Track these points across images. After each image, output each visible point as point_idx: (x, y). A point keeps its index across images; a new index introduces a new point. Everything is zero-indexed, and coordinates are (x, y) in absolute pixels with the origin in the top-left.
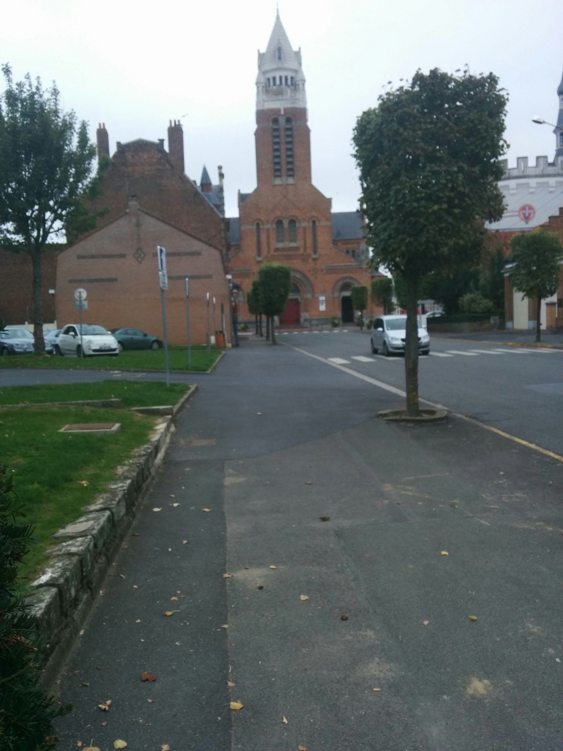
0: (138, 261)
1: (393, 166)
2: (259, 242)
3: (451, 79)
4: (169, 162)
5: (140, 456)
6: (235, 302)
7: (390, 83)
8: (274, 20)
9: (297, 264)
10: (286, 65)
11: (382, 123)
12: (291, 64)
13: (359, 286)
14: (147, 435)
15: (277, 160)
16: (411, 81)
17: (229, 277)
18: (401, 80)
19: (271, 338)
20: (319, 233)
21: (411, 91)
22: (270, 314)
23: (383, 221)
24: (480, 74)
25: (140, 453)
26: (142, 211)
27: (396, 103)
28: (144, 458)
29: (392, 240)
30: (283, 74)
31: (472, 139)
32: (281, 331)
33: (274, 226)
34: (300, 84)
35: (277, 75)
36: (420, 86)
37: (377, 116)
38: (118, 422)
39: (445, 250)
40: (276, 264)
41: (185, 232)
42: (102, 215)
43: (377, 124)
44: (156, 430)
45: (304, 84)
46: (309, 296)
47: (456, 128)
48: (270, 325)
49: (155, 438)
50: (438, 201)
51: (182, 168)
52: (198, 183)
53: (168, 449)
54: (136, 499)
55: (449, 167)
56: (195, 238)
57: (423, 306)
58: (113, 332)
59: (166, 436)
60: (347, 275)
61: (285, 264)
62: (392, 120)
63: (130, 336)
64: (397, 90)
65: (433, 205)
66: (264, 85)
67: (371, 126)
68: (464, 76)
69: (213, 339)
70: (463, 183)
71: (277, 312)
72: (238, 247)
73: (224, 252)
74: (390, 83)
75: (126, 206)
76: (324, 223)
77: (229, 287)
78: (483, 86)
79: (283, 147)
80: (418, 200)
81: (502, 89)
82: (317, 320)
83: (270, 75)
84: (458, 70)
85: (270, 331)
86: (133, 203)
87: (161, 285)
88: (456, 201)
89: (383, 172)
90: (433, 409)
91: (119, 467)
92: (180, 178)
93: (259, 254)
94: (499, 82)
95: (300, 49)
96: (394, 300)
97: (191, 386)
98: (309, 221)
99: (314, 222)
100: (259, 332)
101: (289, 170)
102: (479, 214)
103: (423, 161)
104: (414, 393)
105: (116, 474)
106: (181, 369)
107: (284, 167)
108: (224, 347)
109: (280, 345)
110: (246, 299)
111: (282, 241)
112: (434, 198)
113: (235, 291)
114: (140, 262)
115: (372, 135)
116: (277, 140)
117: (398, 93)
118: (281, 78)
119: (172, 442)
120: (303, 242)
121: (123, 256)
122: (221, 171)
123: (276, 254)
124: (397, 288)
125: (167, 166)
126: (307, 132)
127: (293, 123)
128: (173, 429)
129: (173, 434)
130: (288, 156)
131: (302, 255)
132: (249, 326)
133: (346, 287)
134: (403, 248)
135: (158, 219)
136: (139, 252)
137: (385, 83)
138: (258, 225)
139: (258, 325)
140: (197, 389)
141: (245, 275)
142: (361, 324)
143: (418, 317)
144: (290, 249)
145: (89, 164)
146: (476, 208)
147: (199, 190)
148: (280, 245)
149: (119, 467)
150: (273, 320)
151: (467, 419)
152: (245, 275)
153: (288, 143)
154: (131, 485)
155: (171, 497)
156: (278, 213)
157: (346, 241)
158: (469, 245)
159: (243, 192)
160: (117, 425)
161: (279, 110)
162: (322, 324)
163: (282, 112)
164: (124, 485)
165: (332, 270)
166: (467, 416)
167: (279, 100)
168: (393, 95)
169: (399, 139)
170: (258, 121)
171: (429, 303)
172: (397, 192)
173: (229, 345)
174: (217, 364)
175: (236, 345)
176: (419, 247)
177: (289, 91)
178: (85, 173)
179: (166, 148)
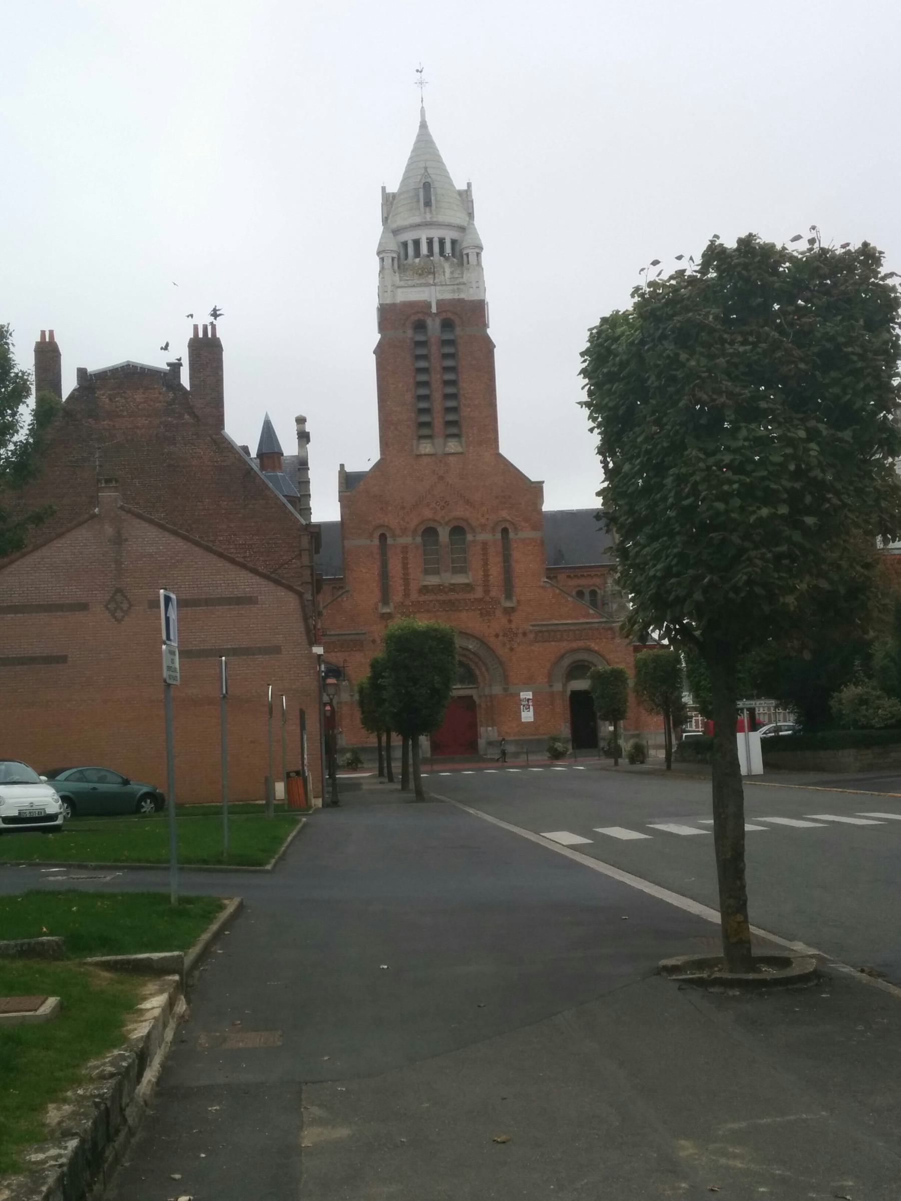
0: (115, 617)
1: (668, 427)
2: (384, 575)
3: (783, 256)
4: (191, 410)
5: (103, 1077)
6: (331, 704)
7: (655, 263)
8: (416, 130)
9: (470, 621)
10: (441, 218)
11: (642, 342)
12: (453, 215)
13: (608, 668)
14: (123, 1024)
15: (423, 391)
16: (698, 260)
17: (318, 650)
18: (679, 258)
19: (412, 785)
20: (516, 555)
21: (701, 280)
22: (410, 732)
23: (653, 538)
24: (843, 247)
25: (104, 1070)
26: (129, 511)
27: (669, 303)
28: (112, 1082)
29: (673, 580)
30: (436, 234)
31: (833, 374)
32: (436, 767)
33: (419, 539)
34: (472, 253)
35: (423, 235)
36: (718, 269)
37: (631, 326)
38: (53, 994)
39: (790, 600)
40: (422, 623)
41: (221, 555)
42: (38, 519)
43: (632, 343)
44: (142, 1012)
45: (478, 254)
46: (497, 690)
47: (797, 353)
48: (410, 754)
49: (140, 1030)
50: (769, 498)
51: (219, 421)
52: (254, 453)
53: (168, 1057)
54: (90, 1186)
55: (789, 430)
56: (244, 566)
57: (752, 711)
58: (52, 775)
59: (165, 1026)
60: (581, 644)
61: (442, 623)
62: (663, 337)
63: (91, 785)
64: (671, 278)
65: (759, 508)
66: (395, 255)
67: (621, 347)
68: (810, 250)
69: (280, 789)
70: (820, 463)
71: (426, 726)
72: (339, 585)
73: (308, 596)
74: (655, 263)
75: (94, 500)
76: (527, 533)
77: (320, 672)
78: (851, 269)
79: (436, 379)
80: (724, 497)
81: (892, 275)
82: (516, 742)
83: (409, 237)
84: (797, 238)
85: (411, 770)
86: (108, 495)
87: (165, 674)
88: (808, 499)
89: (649, 438)
90: (785, 954)
91: (51, 1106)
92: (214, 442)
93: (385, 601)
94: (883, 261)
95: (469, 185)
96: (687, 698)
97: (226, 902)
98: (493, 530)
99: (505, 531)
100: (386, 770)
101: (449, 424)
102: (858, 526)
103: (733, 417)
104: (739, 917)
105: (44, 1125)
106: (205, 862)
107: (438, 421)
108: (306, 807)
109: (433, 800)
110: (357, 697)
111: (436, 572)
112: (759, 494)
113: (331, 681)
114: (119, 621)
115: (623, 365)
116: (422, 364)
117: (673, 282)
118: (430, 242)
119: (179, 1040)
120: (481, 573)
121: (83, 607)
122: (304, 428)
123: (422, 599)
124: (691, 673)
125: (187, 417)
126: (488, 347)
127: (458, 331)
128: (182, 1007)
129: (183, 1021)
130: (447, 397)
131: (480, 600)
132: (363, 757)
133: (578, 669)
134: (698, 596)
135: (162, 527)
136: (119, 597)
137: (647, 263)
138: (383, 537)
139: (383, 755)
140: (241, 907)
141: (356, 644)
142: (614, 752)
143: (740, 736)
144: (453, 588)
145: (14, 414)
146: (850, 515)
147: (255, 466)
148: (433, 580)
149: (51, 1106)
150: (416, 745)
151: (864, 977)
152: (356, 644)
153: (447, 369)
154: (77, 1151)
155: (174, 1179)
156: (428, 513)
157: (576, 572)
158: (842, 591)
159: (349, 469)
160: (52, 1001)
161: (428, 305)
162: (527, 753)
163: (434, 310)
164: (62, 1152)
165: (546, 634)
166: (862, 971)
167: (428, 285)
168: (664, 286)
169: (680, 374)
170: (382, 327)
171: (763, 707)
172: (680, 480)
173: (318, 802)
174: (288, 847)
175: (333, 803)
176: (731, 595)
177: (447, 266)
178: (4, 434)
179: (185, 380)
